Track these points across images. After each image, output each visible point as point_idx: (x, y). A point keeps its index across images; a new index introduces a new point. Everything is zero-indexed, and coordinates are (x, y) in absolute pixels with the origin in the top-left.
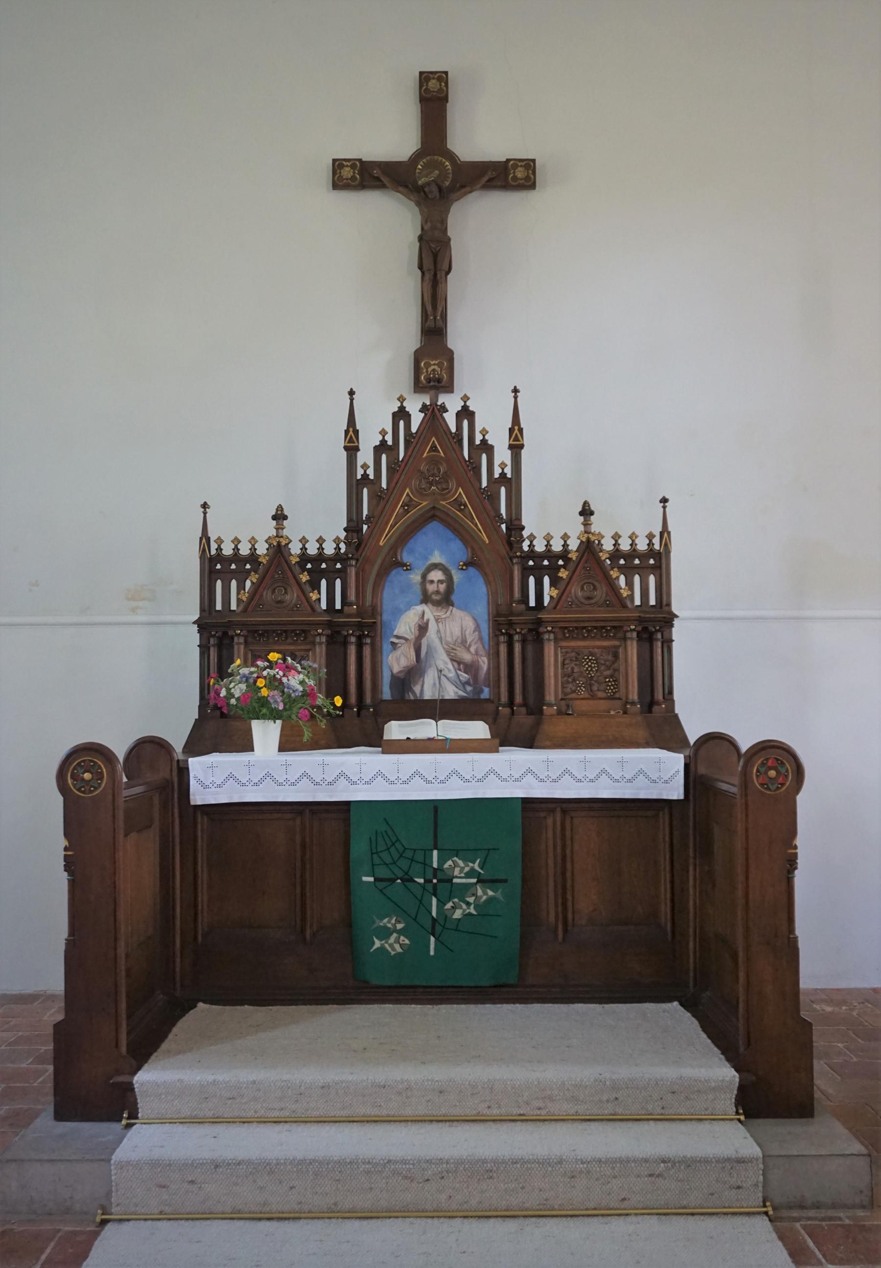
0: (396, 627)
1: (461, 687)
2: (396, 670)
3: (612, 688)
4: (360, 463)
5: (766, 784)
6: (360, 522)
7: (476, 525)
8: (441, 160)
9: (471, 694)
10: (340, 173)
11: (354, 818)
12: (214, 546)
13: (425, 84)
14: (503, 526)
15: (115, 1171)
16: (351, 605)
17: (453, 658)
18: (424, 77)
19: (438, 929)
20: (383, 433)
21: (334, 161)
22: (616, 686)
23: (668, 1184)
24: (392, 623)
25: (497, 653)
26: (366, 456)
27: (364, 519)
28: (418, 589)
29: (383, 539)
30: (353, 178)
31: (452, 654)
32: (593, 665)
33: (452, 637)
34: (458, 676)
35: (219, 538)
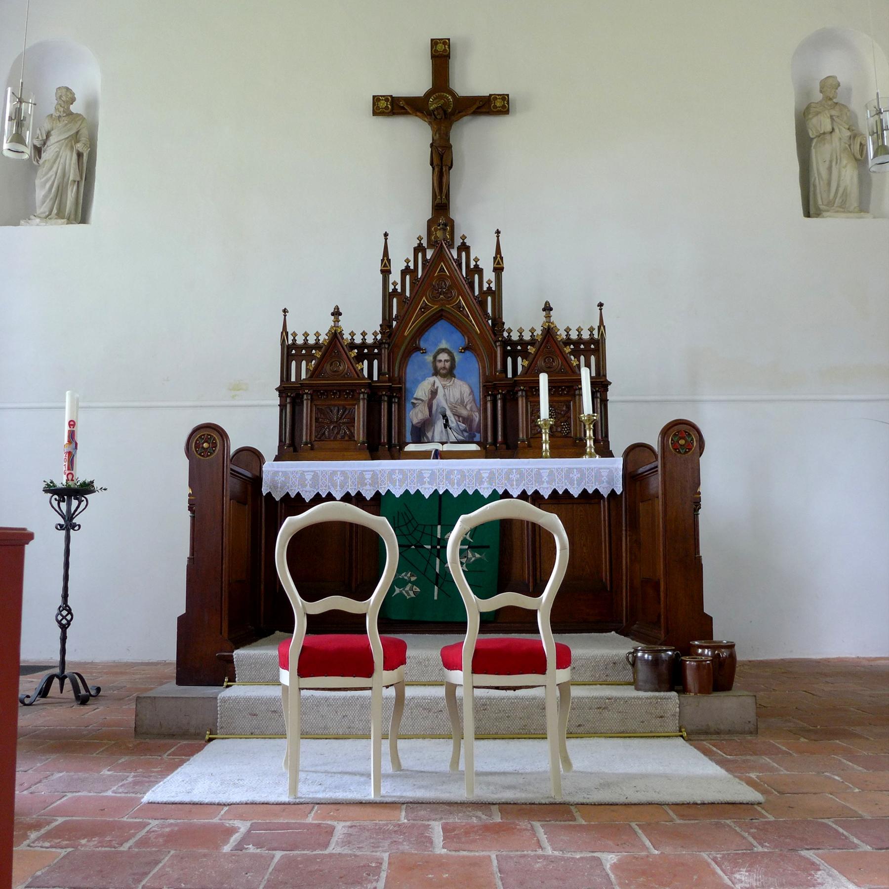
0: (415, 392)
1: (461, 433)
2: (415, 421)
3: (566, 429)
4: (391, 281)
5: (678, 449)
6: (391, 319)
7: (471, 321)
8: (446, 96)
9: (467, 439)
10: (378, 104)
11: (364, 741)
12: (291, 338)
13: (435, 47)
14: (490, 322)
15: (220, 704)
16: (384, 374)
17: (455, 413)
18: (434, 42)
19: (440, 581)
20: (407, 261)
21: (374, 97)
22: (568, 428)
23: (611, 715)
24: (413, 389)
25: (485, 410)
26: (395, 276)
27: (394, 317)
28: (431, 366)
29: (407, 331)
30: (386, 108)
31: (454, 411)
32: (552, 414)
33: (454, 398)
34: (458, 426)
35: (294, 332)
